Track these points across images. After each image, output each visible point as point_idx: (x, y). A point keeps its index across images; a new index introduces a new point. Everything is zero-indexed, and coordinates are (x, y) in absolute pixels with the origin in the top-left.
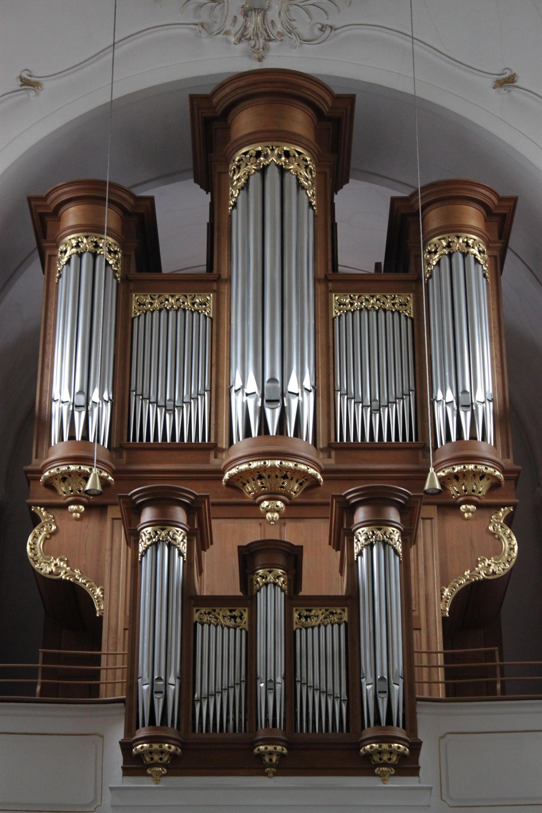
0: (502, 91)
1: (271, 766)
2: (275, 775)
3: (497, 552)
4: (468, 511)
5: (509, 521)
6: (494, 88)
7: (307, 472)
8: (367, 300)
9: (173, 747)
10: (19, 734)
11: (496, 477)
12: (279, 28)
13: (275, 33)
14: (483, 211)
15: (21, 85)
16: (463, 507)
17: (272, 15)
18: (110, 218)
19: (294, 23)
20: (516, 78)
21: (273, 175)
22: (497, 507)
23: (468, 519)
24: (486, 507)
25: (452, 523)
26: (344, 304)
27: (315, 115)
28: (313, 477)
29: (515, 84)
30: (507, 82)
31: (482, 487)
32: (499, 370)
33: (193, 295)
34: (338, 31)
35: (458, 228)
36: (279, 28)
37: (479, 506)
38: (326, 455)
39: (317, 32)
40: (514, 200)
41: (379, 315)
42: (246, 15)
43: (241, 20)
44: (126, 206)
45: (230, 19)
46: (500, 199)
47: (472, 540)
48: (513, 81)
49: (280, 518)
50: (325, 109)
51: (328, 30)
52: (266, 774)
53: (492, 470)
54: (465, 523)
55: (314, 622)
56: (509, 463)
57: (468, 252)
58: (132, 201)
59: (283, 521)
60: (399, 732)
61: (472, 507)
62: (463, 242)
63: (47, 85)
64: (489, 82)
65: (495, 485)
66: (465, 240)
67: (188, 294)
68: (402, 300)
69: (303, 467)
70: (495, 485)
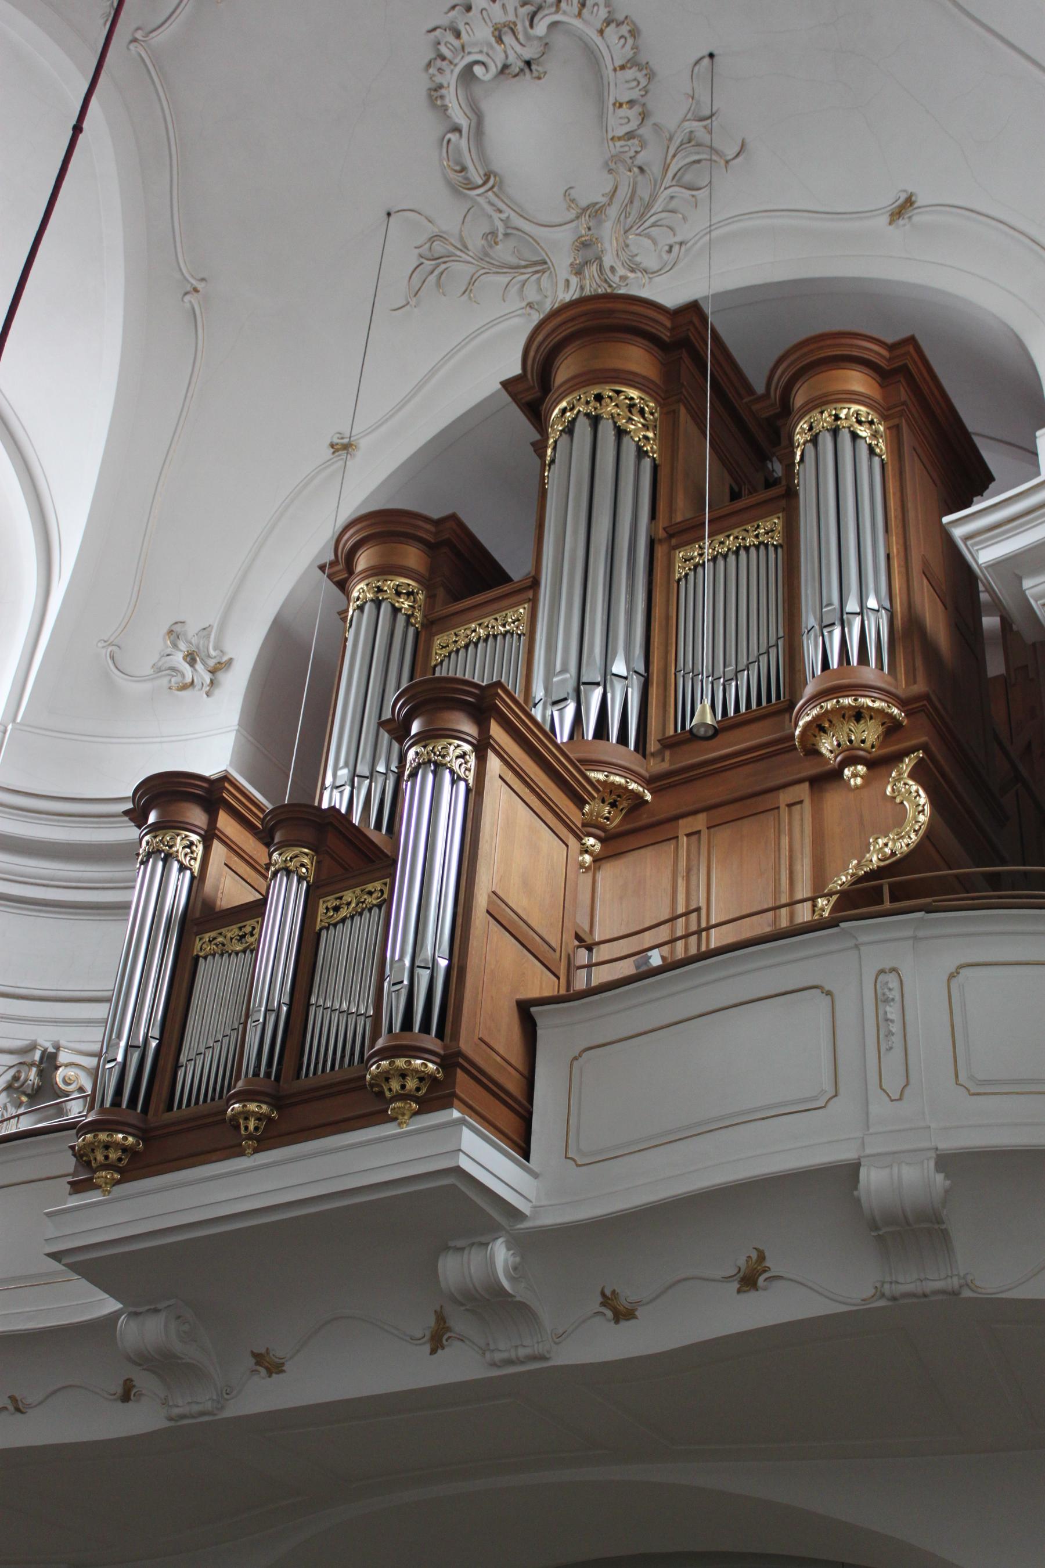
0: (901, 222)
1: (250, 1137)
2: (256, 1151)
3: (899, 818)
4: (855, 775)
5: (915, 774)
6: (890, 224)
7: (626, 788)
8: (722, 543)
9: (130, 1139)
10: (40, 1180)
11: (891, 716)
12: (621, 271)
13: (617, 279)
14: (867, 371)
15: (334, 453)
16: (847, 772)
17: (608, 260)
18: (413, 556)
19: (638, 259)
20: (913, 198)
21: (583, 428)
22: (897, 758)
23: (857, 787)
24: (880, 764)
25: (834, 800)
26: (692, 558)
27: (651, 345)
28: (638, 797)
29: (916, 205)
30: (904, 208)
31: (869, 733)
32: (903, 570)
33: (504, 614)
34: (689, 245)
35: (824, 399)
36: (621, 271)
37: (872, 764)
38: (658, 759)
39: (665, 256)
40: (912, 340)
41: (740, 557)
42: (579, 272)
43: (574, 280)
44: (424, 536)
45: (561, 285)
46: (891, 347)
47: (861, 816)
48: (912, 204)
49: (594, 861)
50: (665, 336)
51: (676, 248)
52: (242, 1154)
53: (883, 704)
54: (851, 795)
55: (344, 912)
56: (902, 688)
57: (838, 426)
58: (432, 529)
59: (598, 864)
60: (430, 1042)
61: (861, 769)
62: (830, 415)
63: (363, 443)
64: (885, 219)
65: (892, 728)
66: (834, 412)
67: (497, 616)
68: (769, 526)
69: (618, 780)
70: (892, 728)
